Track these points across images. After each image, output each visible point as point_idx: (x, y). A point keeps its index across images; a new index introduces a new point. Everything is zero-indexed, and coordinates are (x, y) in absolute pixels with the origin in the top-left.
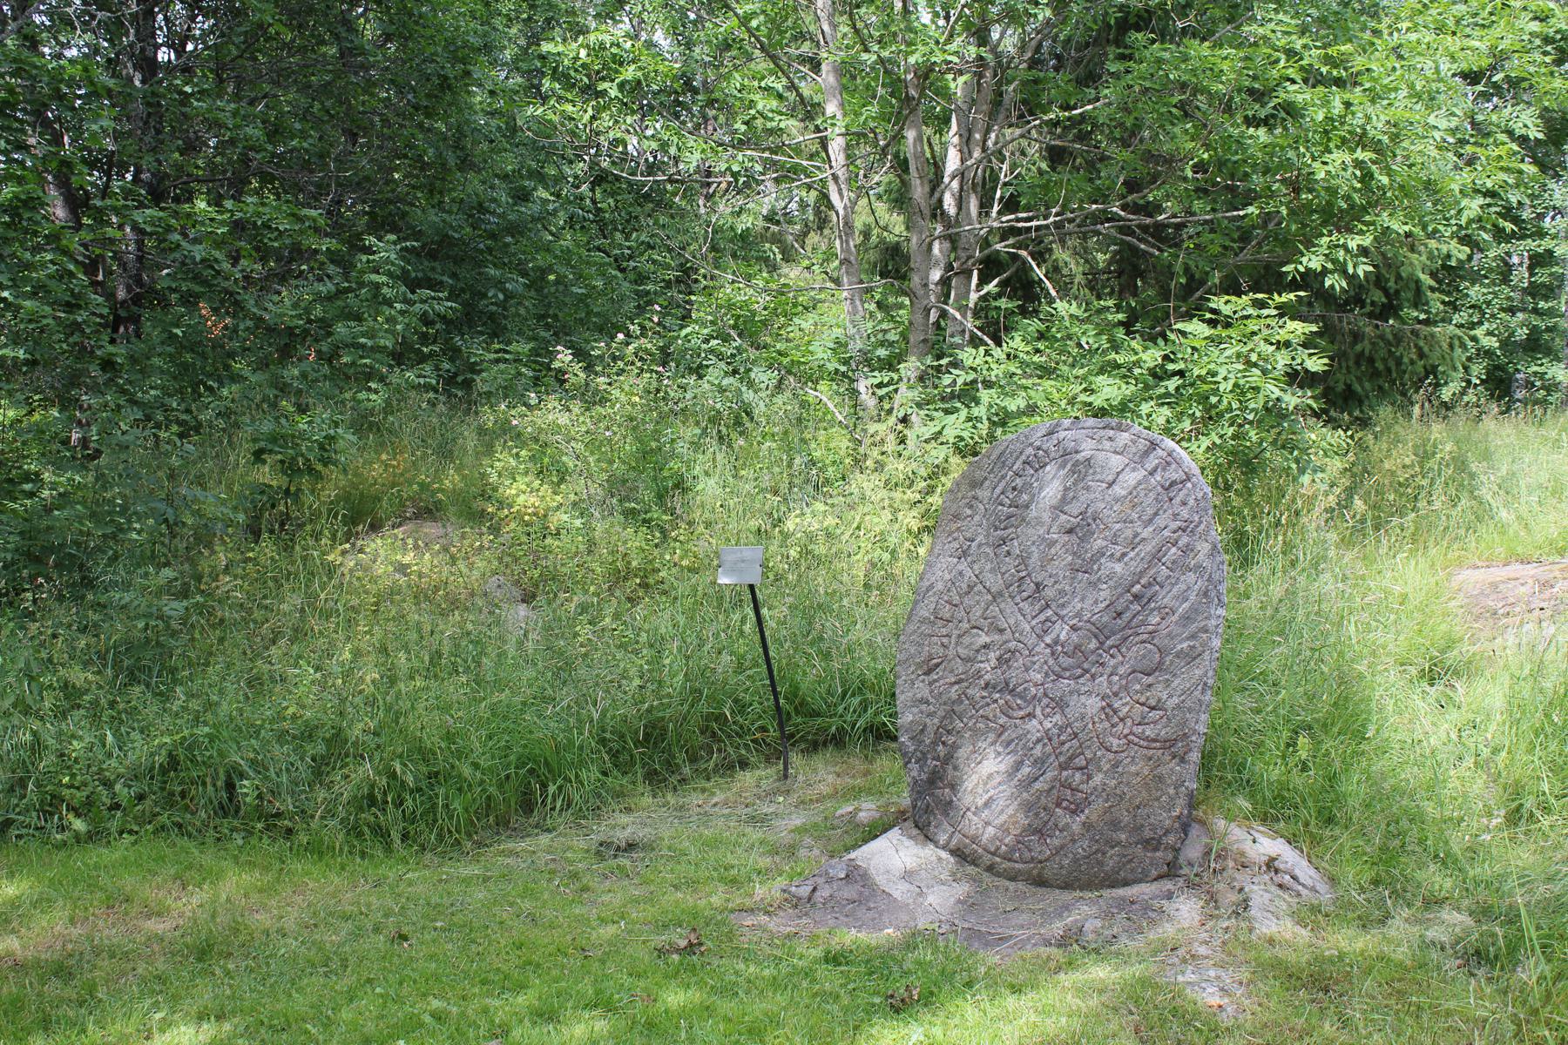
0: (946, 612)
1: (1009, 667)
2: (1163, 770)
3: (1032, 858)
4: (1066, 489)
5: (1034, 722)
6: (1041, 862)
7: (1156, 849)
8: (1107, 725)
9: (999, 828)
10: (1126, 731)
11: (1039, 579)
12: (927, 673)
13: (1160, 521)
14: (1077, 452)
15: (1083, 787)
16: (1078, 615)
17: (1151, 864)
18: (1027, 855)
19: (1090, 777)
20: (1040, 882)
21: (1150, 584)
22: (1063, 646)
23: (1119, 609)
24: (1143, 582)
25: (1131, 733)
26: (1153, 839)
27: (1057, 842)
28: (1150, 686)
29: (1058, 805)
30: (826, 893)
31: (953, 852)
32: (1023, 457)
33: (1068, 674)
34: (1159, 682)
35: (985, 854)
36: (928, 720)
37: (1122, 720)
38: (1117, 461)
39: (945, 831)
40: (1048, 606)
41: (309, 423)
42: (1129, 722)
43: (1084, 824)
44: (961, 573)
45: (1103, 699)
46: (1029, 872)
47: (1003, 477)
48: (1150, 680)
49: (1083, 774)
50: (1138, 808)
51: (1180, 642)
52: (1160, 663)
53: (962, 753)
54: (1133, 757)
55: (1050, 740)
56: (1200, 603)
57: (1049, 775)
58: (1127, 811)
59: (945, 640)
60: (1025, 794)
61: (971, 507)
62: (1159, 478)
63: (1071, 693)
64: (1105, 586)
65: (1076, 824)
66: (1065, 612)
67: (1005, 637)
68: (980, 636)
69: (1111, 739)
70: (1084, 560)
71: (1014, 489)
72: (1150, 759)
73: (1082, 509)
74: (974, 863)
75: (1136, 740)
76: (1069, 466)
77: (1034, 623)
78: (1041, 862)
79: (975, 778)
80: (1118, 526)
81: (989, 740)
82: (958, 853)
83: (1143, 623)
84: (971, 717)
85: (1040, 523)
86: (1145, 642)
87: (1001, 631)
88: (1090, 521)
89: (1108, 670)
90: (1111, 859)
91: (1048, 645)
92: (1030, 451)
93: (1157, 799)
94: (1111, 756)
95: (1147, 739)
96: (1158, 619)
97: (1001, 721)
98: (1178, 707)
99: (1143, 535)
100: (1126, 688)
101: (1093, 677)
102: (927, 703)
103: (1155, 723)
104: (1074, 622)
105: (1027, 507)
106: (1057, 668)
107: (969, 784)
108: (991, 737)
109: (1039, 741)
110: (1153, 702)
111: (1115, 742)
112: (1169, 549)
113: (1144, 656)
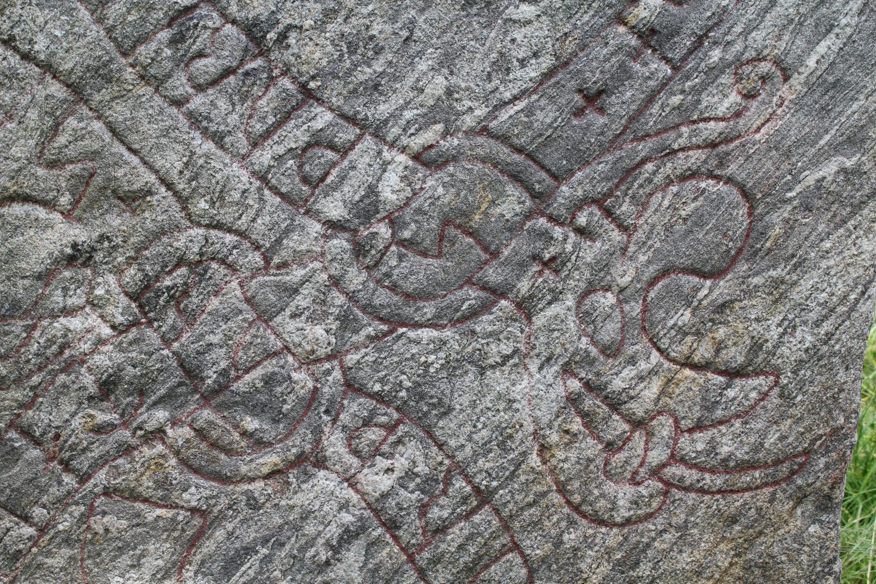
1: (190, 317)
8: (591, 447)
10: (657, 456)
22: (394, 222)
23: (594, 79)
25: (676, 458)
28: (722, 307)
33: (429, 310)
34: (749, 293)
37: (637, 424)
40: (308, 95)
41: (117, 237)
42: (664, 427)
45: (567, 370)
48: (724, 287)
51: (815, 162)
54: (683, 528)
55: (392, 526)
63: (452, 368)
66: (384, 109)
67: (150, 219)
69: (610, 487)
75: (691, 475)
77: (264, 157)
84: (63, 503)
89: (578, 280)
91: (334, 226)
94: (613, 537)
95: (725, 466)
96: (734, 98)
97: (191, 498)
103: (745, 415)
104: (428, 136)
106: (382, 297)
110: (735, 355)
111: (624, 493)
113: (698, 220)
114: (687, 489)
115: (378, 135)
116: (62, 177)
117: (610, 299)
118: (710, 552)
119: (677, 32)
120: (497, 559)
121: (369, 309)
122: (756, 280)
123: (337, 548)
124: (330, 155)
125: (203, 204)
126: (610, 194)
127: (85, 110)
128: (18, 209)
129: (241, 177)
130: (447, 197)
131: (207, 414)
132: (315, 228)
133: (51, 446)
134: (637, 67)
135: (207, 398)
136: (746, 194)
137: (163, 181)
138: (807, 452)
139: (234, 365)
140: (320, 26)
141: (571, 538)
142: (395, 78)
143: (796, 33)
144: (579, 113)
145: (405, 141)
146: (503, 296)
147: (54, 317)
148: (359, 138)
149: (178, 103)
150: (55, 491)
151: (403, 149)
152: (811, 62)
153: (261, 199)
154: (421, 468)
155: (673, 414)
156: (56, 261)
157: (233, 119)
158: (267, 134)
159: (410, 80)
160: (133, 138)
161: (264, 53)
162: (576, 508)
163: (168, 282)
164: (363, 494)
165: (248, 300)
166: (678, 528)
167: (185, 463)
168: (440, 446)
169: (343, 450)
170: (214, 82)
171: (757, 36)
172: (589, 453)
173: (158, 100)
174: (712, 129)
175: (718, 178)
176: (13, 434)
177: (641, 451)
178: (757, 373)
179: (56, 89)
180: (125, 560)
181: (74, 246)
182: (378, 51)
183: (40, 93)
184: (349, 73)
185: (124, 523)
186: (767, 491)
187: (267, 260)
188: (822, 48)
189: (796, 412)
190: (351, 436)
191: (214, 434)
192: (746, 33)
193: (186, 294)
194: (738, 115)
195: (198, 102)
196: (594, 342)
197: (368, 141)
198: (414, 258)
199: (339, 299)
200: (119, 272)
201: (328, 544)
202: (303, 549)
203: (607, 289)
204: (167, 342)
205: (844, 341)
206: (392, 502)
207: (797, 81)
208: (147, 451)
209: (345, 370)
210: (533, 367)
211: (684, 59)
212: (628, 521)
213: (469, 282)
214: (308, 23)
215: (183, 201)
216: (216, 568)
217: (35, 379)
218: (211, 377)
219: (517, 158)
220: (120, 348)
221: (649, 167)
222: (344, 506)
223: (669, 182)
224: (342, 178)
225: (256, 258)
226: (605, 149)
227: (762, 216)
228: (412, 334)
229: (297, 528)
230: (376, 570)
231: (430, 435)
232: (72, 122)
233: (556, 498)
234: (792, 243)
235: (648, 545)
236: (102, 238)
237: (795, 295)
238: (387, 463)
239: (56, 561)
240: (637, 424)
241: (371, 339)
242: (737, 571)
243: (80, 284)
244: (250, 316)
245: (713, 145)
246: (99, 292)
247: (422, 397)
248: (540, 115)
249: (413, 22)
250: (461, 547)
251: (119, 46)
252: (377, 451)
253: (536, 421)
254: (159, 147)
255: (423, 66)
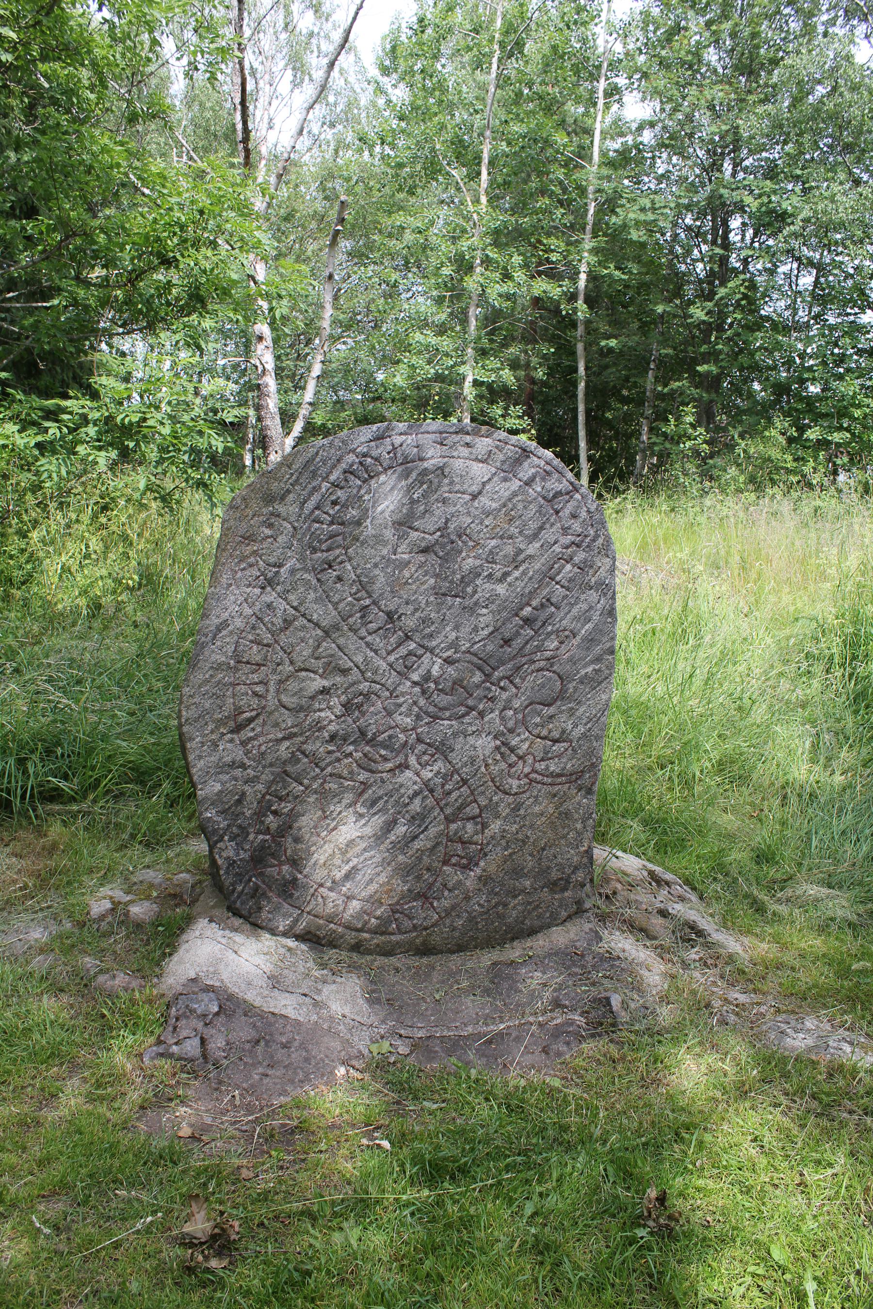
0: (255, 653)
1: (363, 714)
2: (568, 805)
3: (415, 926)
4: (413, 502)
5: (408, 774)
6: (426, 929)
7: (564, 889)
8: (503, 765)
9: (368, 900)
10: (527, 770)
11: (392, 607)
12: (238, 729)
13: (548, 535)
14: (422, 459)
15: (478, 838)
16: (454, 645)
17: (560, 906)
18: (407, 924)
19: (485, 826)
20: (425, 950)
21: (542, 605)
22: (436, 683)
23: (507, 635)
24: (534, 603)
25: (534, 771)
26: (561, 879)
27: (446, 903)
28: (551, 717)
29: (446, 862)
30: (221, 1042)
31: (298, 938)
32: (344, 465)
33: (447, 714)
34: (561, 712)
35: (348, 932)
36: (246, 788)
37: (520, 758)
38: (480, 471)
39: (286, 916)
40: (408, 637)
42: (530, 759)
43: (480, 878)
44: (269, 606)
45: (495, 737)
46: (411, 942)
47: (315, 489)
48: (552, 710)
49: (476, 824)
50: (543, 849)
51: (585, 667)
52: (563, 690)
53: (306, 822)
54: (536, 797)
55: (432, 791)
56: (606, 622)
57: (433, 831)
58: (531, 855)
59: (259, 689)
60: (401, 858)
61: (270, 526)
62: (539, 489)
63: (455, 735)
64: (484, 611)
65: (470, 880)
66: (434, 643)
67: (351, 679)
68: (315, 680)
69: (510, 780)
70: (452, 582)
71: (334, 503)
72: (555, 796)
73: (441, 523)
74: (332, 945)
75: (539, 778)
76: (414, 475)
77: (392, 658)
78: (426, 929)
79: (328, 848)
80: (493, 543)
81: (345, 801)
82: (309, 938)
83: (539, 649)
85: (379, 540)
86: (542, 669)
87: (345, 672)
88: (453, 537)
89: (500, 705)
90: (514, 909)
91: (415, 683)
92: (351, 458)
93: (564, 837)
94: (511, 799)
95: (552, 775)
96: (556, 643)
97: (361, 778)
98: (584, 735)
99: (528, 552)
100: (524, 722)
101: (481, 714)
102: (243, 766)
103: (559, 756)
104: (449, 653)
105: (359, 523)
107: (320, 856)
108: (348, 797)
109: (416, 794)
110: (556, 734)
111: (515, 783)
112: (563, 566)
113: (543, 686)
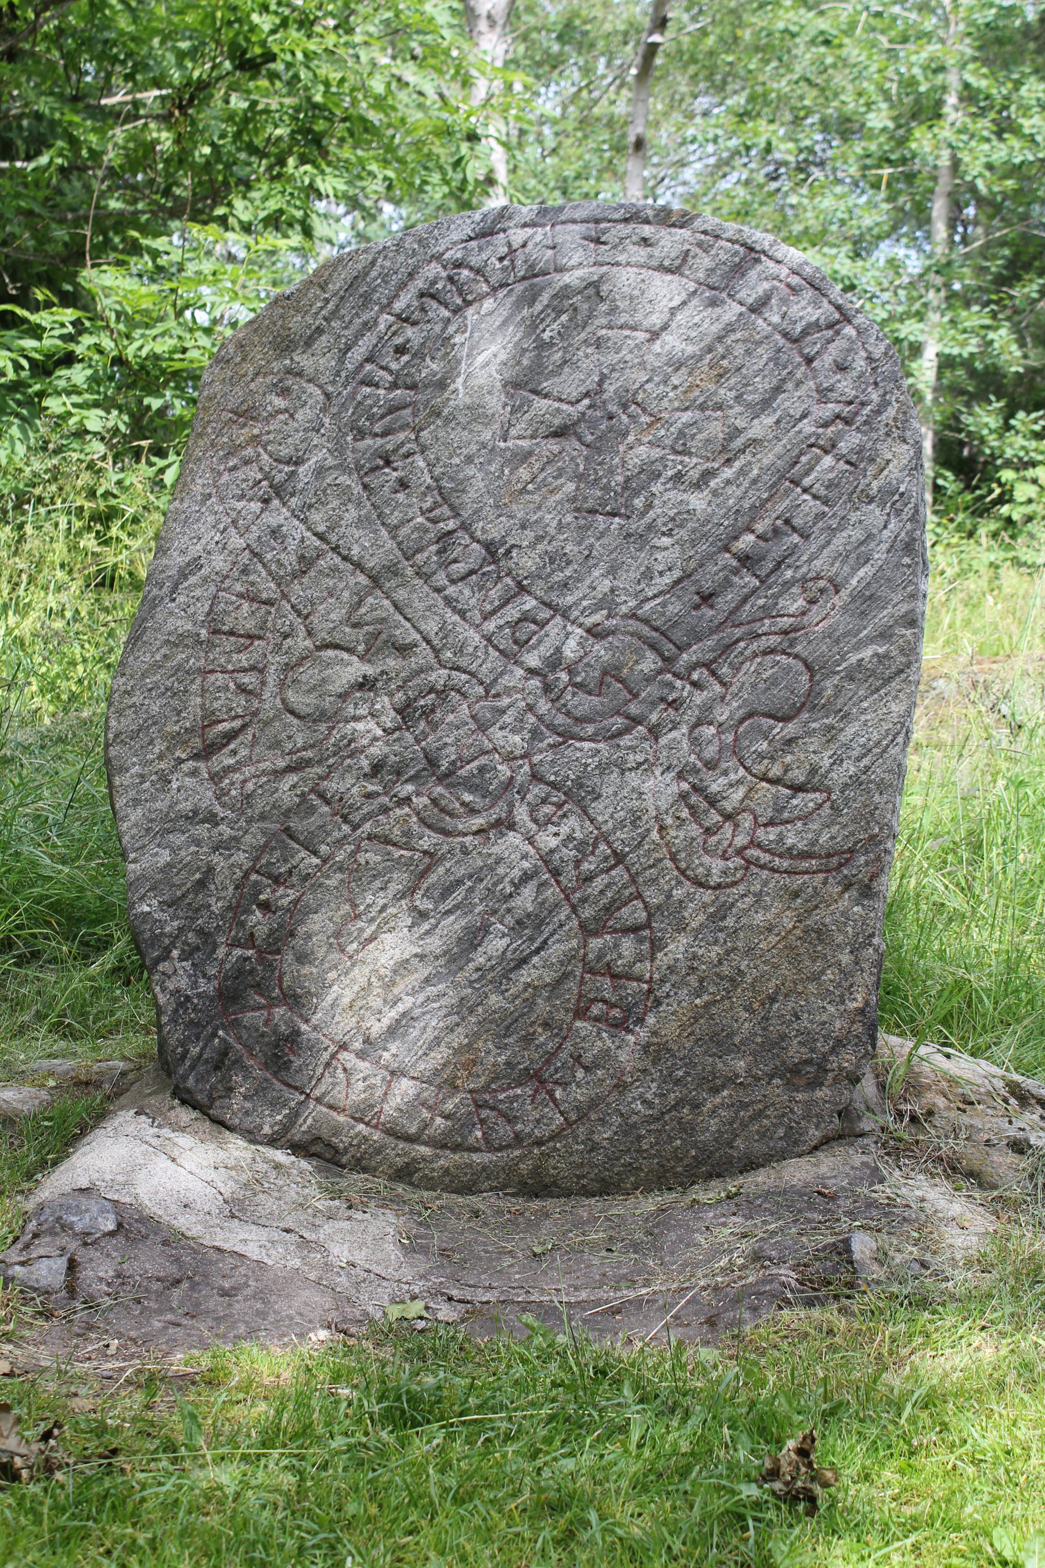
1: (434, 726)
10: (741, 840)
22: (570, 672)
23: (707, 586)
25: (754, 843)
28: (790, 742)
33: (590, 729)
34: (810, 733)
37: (728, 817)
40: (522, 589)
42: (746, 821)
45: (680, 776)
48: (791, 729)
51: (857, 647)
54: (759, 895)
55: (556, 873)
63: (603, 768)
66: (570, 599)
67: (414, 662)
69: (706, 859)
75: (765, 858)
77: (491, 626)
84: (340, 843)
89: (691, 716)
91: (532, 672)
94: (708, 896)
95: (789, 853)
96: (801, 602)
97: (425, 844)
103: (806, 818)
104: (597, 618)
106: (560, 719)
110: (798, 775)
111: (717, 865)
113: (774, 682)
114: (762, 867)
115: (565, 616)
116: (361, 633)
117: (712, 730)
118: (778, 916)
119: (763, 558)
120: (626, 904)
121: (552, 728)
122: (814, 725)
123: (517, 886)
124: (533, 627)
125: (449, 654)
126: (715, 661)
127: (379, 593)
128: (331, 653)
129: (475, 638)
130: (606, 656)
131: (439, 789)
132: (520, 672)
133: (336, 806)
134: (736, 579)
135: (440, 780)
136: (808, 667)
137: (424, 639)
138: (851, 851)
139: (460, 759)
140: (532, 546)
141: (678, 893)
142: (579, 581)
143: (843, 562)
144: (697, 607)
145: (581, 620)
146: (640, 723)
147: (347, 722)
148: (553, 617)
149: (438, 590)
150: (336, 834)
151: (580, 626)
152: (854, 582)
153: (487, 653)
154: (578, 835)
155: (752, 812)
156: (352, 687)
157: (473, 602)
158: (494, 612)
159: (588, 582)
160: (408, 611)
161: (496, 562)
162: (683, 872)
163: (422, 703)
164: (538, 849)
165: (473, 717)
166: (755, 895)
167: (422, 821)
168: (592, 821)
169: (527, 818)
170: (462, 579)
171: (817, 563)
172: (694, 834)
173: (426, 588)
174: (785, 622)
175: (789, 655)
176: (312, 796)
177: (729, 836)
178: (815, 790)
179: (363, 579)
180: (377, 884)
181: (365, 677)
182: (569, 563)
183: (352, 581)
184: (549, 575)
185: (379, 858)
186: (821, 876)
187: (487, 692)
188: (861, 573)
189: (843, 820)
190: (533, 810)
191: (443, 803)
192: (810, 561)
193: (433, 711)
194: (803, 614)
195: (451, 590)
196: (700, 759)
197: (558, 619)
198: (582, 695)
199: (532, 719)
200: (391, 695)
201: (512, 882)
202: (495, 885)
203: (710, 723)
204: (418, 741)
205: (878, 773)
206: (557, 856)
207: (844, 593)
208: (398, 811)
209: (532, 766)
210: (658, 773)
211: (768, 576)
212: (718, 886)
213: (618, 713)
214: (525, 543)
215: (436, 652)
216: (436, 894)
217: (331, 761)
218: (444, 765)
219: (654, 634)
220: (387, 743)
221: (742, 644)
222: (525, 856)
223: (755, 655)
224: (540, 642)
225: (481, 690)
226: (712, 632)
227: (819, 683)
228: (578, 745)
229: (492, 869)
230: (543, 903)
231: (586, 813)
232: (370, 600)
233: (668, 863)
234: (840, 701)
235: (733, 905)
236: (383, 673)
237: (842, 738)
238: (555, 829)
239: (332, 882)
240: (728, 817)
241: (551, 746)
242: (798, 932)
243: (366, 701)
244: (473, 727)
245: (786, 633)
246: (378, 706)
247: (581, 786)
248: (670, 607)
249: (592, 545)
250: (602, 892)
251: (404, 554)
252: (549, 821)
253: (657, 809)
254: (424, 617)
255: (596, 573)
